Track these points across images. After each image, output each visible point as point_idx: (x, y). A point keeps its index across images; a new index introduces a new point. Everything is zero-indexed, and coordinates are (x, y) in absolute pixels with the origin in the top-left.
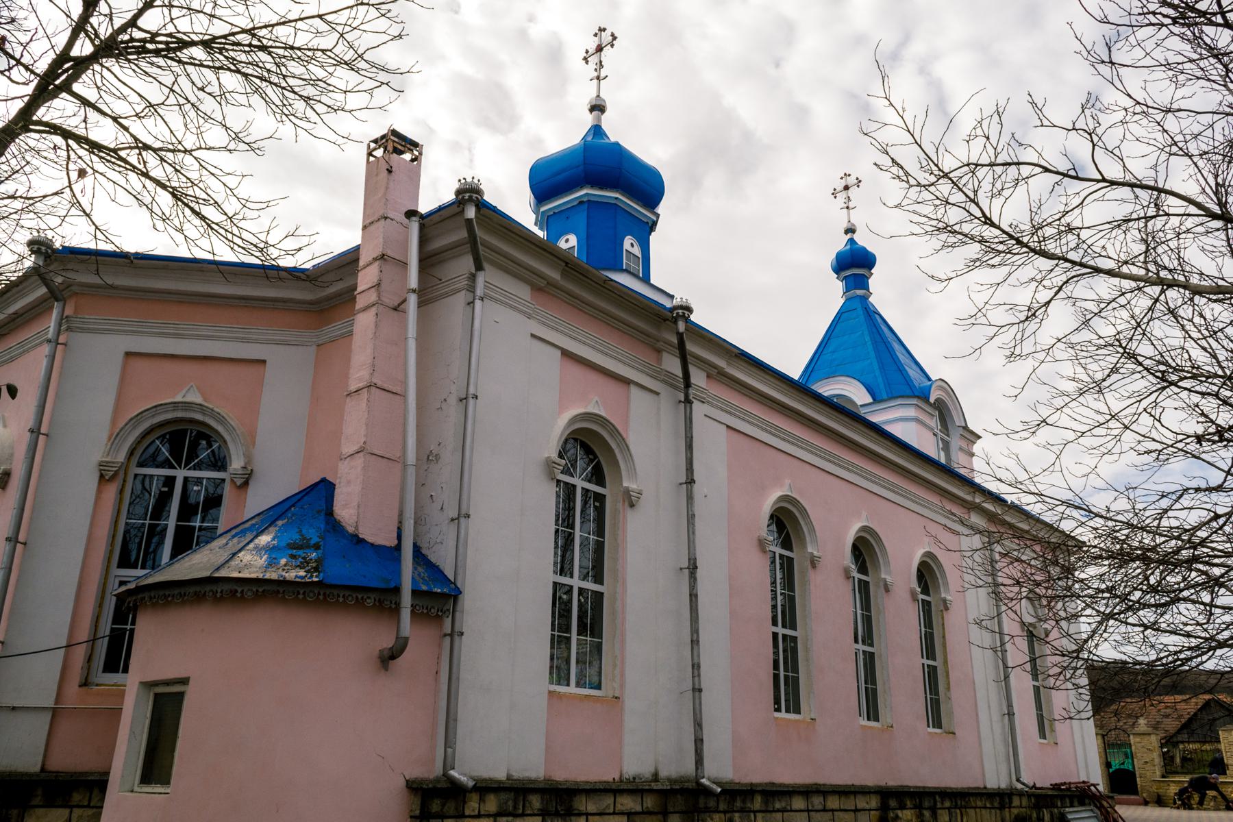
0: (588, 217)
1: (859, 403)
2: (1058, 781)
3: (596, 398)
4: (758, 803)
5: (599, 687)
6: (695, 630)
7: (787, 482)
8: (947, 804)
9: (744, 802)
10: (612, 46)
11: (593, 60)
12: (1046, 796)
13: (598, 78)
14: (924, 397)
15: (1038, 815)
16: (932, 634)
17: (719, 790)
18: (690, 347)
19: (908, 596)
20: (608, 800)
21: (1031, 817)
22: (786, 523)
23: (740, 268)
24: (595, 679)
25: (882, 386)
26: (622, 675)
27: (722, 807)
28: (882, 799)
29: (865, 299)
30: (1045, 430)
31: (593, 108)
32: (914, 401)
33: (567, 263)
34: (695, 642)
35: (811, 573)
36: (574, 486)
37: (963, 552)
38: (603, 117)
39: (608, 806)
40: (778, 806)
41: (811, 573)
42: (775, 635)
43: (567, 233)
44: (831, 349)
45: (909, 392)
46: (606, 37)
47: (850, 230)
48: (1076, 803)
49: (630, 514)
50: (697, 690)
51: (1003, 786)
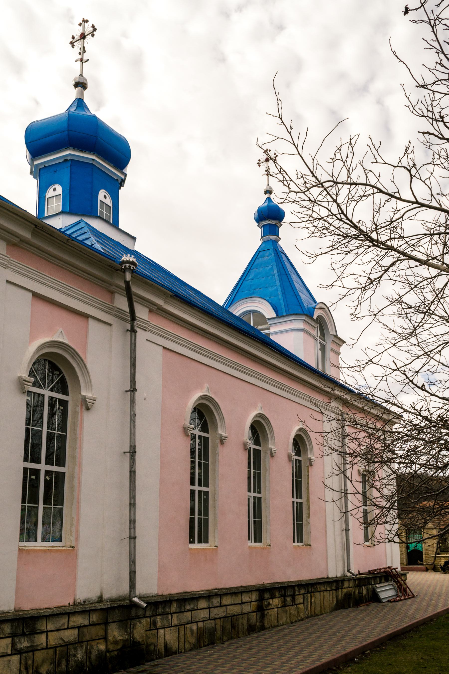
0: (71, 173)
1: (267, 317)
2: (373, 569)
3: (61, 330)
4: (174, 607)
5: (60, 540)
6: (133, 497)
7: (206, 385)
8: (302, 591)
9: (164, 608)
10: (93, 35)
11: (78, 45)
12: (365, 578)
13: (81, 60)
14: (310, 316)
15: (359, 590)
16: (301, 482)
17: (145, 605)
18: (135, 289)
19: (286, 459)
20: (64, 620)
21: (354, 593)
22: (204, 413)
23: (184, 218)
24: (58, 534)
25: (283, 306)
26: (77, 531)
27: (148, 613)
28: (260, 594)
29: (275, 242)
30: (371, 367)
31: (77, 85)
32: (303, 318)
33: (36, 226)
34: (132, 505)
35: (220, 447)
36: (43, 396)
37: (323, 426)
38: (85, 92)
39: (64, 624)
40: (188, 608)
41: (220, 447)
42: (192, 492)
43: (55, 183)
44: (250, 277)
45: (300, 311)
46: (88, 28)
47: (268, 192)
48: (383, 581)
49: (86, 415)
50: (133, 538)
51: (339, 575)
